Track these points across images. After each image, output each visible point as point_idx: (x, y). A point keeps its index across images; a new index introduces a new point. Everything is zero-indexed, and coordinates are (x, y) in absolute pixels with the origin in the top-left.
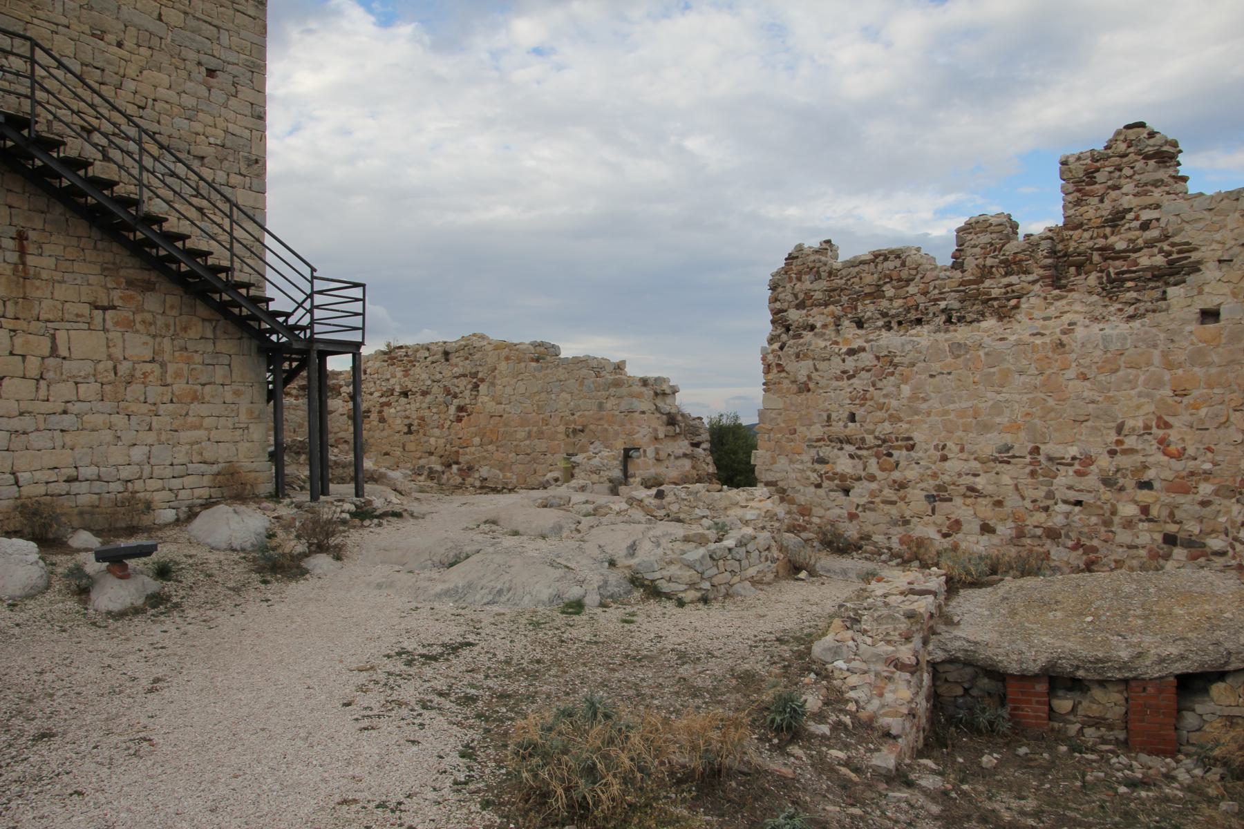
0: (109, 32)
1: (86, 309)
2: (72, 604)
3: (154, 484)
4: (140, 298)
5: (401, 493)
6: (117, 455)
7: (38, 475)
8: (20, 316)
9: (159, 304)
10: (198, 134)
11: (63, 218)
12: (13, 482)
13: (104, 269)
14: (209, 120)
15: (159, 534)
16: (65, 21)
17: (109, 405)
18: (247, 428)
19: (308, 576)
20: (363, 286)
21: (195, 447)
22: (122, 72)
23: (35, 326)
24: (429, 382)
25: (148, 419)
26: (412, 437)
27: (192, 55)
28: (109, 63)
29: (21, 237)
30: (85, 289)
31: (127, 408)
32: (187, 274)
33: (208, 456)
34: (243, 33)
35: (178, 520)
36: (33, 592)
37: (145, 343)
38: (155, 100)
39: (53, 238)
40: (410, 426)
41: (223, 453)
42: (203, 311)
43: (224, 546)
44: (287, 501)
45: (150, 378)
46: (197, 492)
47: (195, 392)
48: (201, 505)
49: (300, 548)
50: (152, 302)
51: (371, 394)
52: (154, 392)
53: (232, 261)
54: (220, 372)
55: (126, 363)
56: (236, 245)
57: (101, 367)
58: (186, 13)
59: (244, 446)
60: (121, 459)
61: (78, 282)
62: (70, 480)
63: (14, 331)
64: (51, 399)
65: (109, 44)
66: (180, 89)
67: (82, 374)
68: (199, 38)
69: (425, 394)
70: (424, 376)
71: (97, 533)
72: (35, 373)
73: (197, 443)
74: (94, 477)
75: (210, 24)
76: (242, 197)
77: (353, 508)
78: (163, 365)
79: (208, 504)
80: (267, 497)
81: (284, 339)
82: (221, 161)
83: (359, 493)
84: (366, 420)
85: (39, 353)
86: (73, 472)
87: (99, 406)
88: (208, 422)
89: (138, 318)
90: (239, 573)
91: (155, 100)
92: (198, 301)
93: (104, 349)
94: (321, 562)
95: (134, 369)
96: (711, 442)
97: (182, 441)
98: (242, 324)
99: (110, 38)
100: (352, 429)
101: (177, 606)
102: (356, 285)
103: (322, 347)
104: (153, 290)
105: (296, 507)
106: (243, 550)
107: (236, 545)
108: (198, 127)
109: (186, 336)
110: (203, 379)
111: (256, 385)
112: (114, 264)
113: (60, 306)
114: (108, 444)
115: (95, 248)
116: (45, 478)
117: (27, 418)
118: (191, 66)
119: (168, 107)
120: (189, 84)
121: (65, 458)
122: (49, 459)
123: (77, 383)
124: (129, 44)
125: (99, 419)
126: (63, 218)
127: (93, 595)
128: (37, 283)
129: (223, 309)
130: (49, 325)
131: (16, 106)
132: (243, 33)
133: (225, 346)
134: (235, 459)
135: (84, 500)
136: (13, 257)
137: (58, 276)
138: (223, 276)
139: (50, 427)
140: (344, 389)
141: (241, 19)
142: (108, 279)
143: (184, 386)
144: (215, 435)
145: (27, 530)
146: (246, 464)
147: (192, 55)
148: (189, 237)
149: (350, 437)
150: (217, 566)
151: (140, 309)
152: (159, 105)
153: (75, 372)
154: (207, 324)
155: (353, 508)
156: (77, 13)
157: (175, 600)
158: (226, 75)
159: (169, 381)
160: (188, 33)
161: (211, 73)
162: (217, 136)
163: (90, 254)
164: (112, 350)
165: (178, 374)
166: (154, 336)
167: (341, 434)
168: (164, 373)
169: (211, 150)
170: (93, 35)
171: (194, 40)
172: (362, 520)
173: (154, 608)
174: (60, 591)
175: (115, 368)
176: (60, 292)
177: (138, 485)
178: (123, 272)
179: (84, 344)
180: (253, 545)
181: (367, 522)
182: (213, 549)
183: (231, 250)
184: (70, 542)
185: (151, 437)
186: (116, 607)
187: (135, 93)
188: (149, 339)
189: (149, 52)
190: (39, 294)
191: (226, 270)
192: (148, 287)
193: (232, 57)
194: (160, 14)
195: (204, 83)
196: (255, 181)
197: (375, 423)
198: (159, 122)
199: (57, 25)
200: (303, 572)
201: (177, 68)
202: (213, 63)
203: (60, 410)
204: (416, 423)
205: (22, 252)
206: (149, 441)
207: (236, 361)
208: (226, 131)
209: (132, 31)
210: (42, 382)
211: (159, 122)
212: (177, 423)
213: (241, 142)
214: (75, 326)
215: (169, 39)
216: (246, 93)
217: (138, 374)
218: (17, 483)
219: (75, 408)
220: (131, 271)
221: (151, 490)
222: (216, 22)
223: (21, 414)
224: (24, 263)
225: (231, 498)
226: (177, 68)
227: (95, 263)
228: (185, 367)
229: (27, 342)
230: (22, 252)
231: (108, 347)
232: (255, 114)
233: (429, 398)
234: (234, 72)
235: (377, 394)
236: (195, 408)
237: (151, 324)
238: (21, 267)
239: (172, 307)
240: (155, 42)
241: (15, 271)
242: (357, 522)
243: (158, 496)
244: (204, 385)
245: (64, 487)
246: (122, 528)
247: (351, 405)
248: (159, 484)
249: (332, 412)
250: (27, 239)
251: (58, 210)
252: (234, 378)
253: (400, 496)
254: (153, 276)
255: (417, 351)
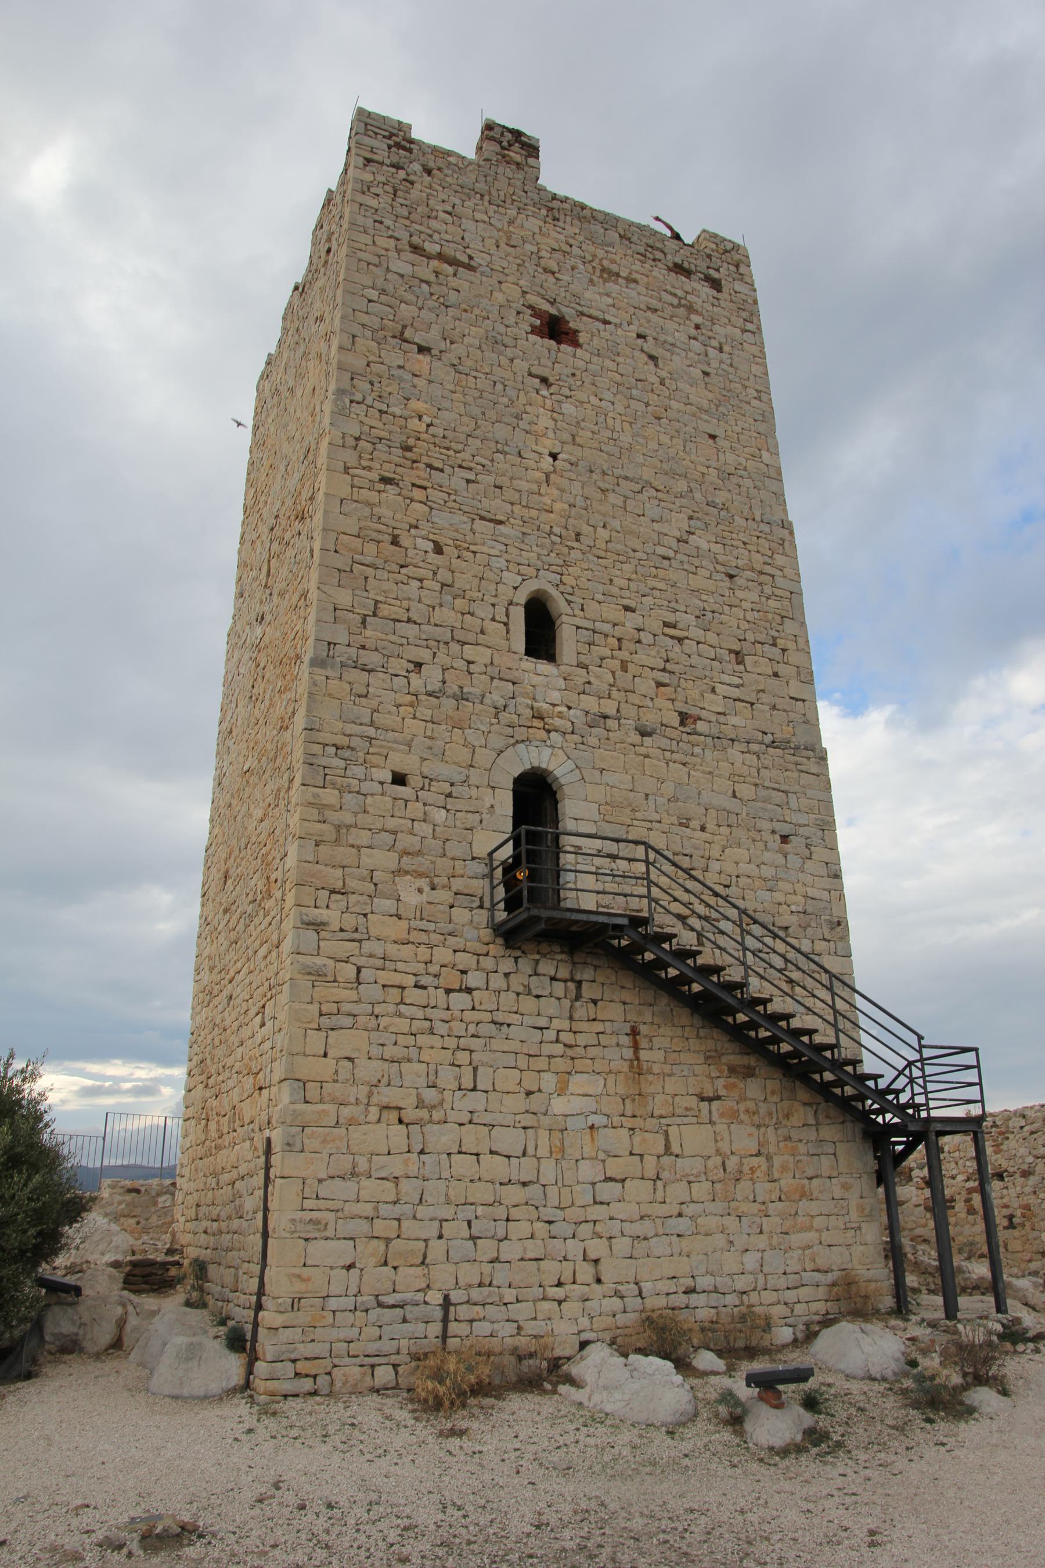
0: (695, 819)
1: (693, 1102)
2: (726, 1435)
3: (769, 1297)
4: (742, 1085)
5: (1034, 1309)
6: (731, 1262)
7: (659, 1284)
8: (637, 1113)
9: (761, 1090)
10: (780, 904)
11: (668, 1009)
12: (637, 1293)
13: (707, 1058)
14: (788, 887)
15: (780, 1356)
16: (657, 817)
17: (719, 1206)
18: (859, 1228)
19: (976, 1415)
20: (976, 1050)
21: (807, 1252)
22: (707, 855)
23: (651, 1123)
24: (1030, 1159)
25: (758, 1220)
26: (1016, 1233)
27: (766, 825)
28: (696, 849)
29: (634, 1033)
30: (692, 1080)
31: (737, 1209)
32: (789, 1055)
33: (821, 1262)
34: (810, 793)
35: (795, 1340)
36: (683, 1419)
37: (750, 1135)
38: (738, 877)
39: (661, 1030)
40: (1010, 1217)
41: (834, 1258)
42: (803, 1094)
43: (860, 1373)
44: (913, 1318)
45: (758, 1173)
46: (816, 1306)
47: (803, 1186)
48: (819, 1322)
49: (956, 1379)
50: (753, 1088)
51: (953, 1178)
52: (763, 1189)
53: (837, 1038)
54: (826, 1162)
55: (732, 1157)
56: (831, 1018)
57: (711, 1163)
58: (756, 785)
59: (858, 1250)
60: (736, 1268)
61: (685, 1073)
62: (690, 1291)
63: (633, 1129)
64: (667, 1200)
65: (694, 830)
66: (759, 861)
67: (694, 1172)
68: (770, 807)
69: (1026, 1174)
70: (1022, 1151)
71: (720, 1354)
72: (651, 1173)
73: (809, 1247)
74: (711, 1288)
75: (778, 790)
76: (832, 964)
77: (999, 1327)
78: (769, 1158)
79: (827, 1322)
80: (889, 1314)
81: (896, 1120)
82: (805, 928)
83: (1001, 1307)
84: (950, 1212)
85: (655, 1152)
86: (689, 1282)
87: (711, 1207)
88: (818, 1222)
89: (742, 1107)
90: (891, 1408)
91: (738, 877)
92: (798, 1083)
93: (713, 1144)
94: (983, 1397)
95: (741, 1164)
96: (948, 1224)
97: (793, 1246)
98: (845, 1104)
99: (695, 824)
100: (932, 1224)
101: (839, 1445)
102: (965, 1050)
103: (939, 1127)
104: (753, 1075)
105: (929, 1325)
106: (884, 1379)
107: (875, 1372)
108: (779, 897)
109: (789, 1124)
110: (810, 1173)
111: (865, 1176)
112: (716, 1051)
113: (670, 1100)
114: (722, 1249)
115: (698, 1037)
116: (665, 1290)
117: (647, 1222)
118: (766, 836)
119: (750, 881)
120: (767, 854)
121: (682, 1266)
122: (668, 1268)
123: (689, 1182)
124: (711, 826)
125: (712, 1222)
126: (668, 1009)
127: (748, 1426)
128: (650, 1077)
129: (824, 1090)
130: (663, 1121)
131: (624, 905)
132: (810, 793)
133: (829, 1132)
134: (849, 1266)
135: (704, 1314)
136: (629, 1053)
137: (667, 1069)
138: (828, 1054)
139: (667, 1231)
140: (915, 1173)
141: (805, 779)
142: (712, 1067)
143: (792, 1181)
144: (826, 1237)
145: (655, 1348)
146: (862, 1272)
147: (766, 825)
148: (794, 1016)
149: (932, 1235)
150: (862, 1397)
151: (743, 1098)
152: (743, 881)
153: (687, 1171)
154: (808, 1108)
155: (999, 1327)
156: (666, 807)
157: (836, 1437)
158: (798, 839)
159: (776, 1176)
160: (760, 804)
161: (785, 839)
162: (798, 902)
163: (694, 1044)
164: (720, 1144)
165: (784, 1168)
166: (758, 1126)
167: (919, 1231)
168: (770, 1167)
169: (794, 919)
170: (681, 824)
171: (765, 810)
172: (1014, 1344)
173: (815, 1446)
174: (709, 1420)
175: (723, 1163)
176: (672, 1085)
177: (754, 1297)
178: (724, 1059)
179: (693, 1138)
180: (895, 1374)
181: (1020, 1347)
182: (848, 1377)
183: (835, 1025)
184: (695, 1363)
185: (762, 1242)
186: (778, 1442)
187: (720, 873)
188: (753, 1130)
189: (728, 830)
190: (652, 1089)
191: (831, 1047)
192: (749, 1073)
193: (802, 819)
194: (734, 791)
195: (779, 851)
196: (840, 945)
197: (963, 1215)
198: (743, 898)
199: (651, 822)
200: (969, 1412)
201: (754, 841)
202: (785, 829)
203: (676, 1213)
204: (1018, 1213)
205: (636, 1047)
206: (761, 1246)
207: (842, 1149)
208: (806, 897)
209: (712, 812)
210: (659, 1182)
211: (743, 898)
212: (788, 1223)
213: (822, 905)
214: (686, 1120)
215: (744, 814)
216: (819, 853)
217: (746, 1169)
218: (640, 1294)
219: (689, 1210)
220: (732, 1057)
221: (764, 1302)
222: (783, 788)
223: (642, 1218)
224: (638, 1059)
225: (849, 1313)
226: (754, 841)
227: (699, 1052)
228: (791, 1159)
229: (644, 1141)
230: (636, 1047)
231: (716, 1141)
232: (832, 873)
233: (1033, 1180)
234: (806, 834)
235: (960, 1178)
236: (804, 1205)
237: (754, 1113)
238: (636, 1063)
239: (773, 1093)
240: (733, 819)
241: (631, 1067)
242: (1008, 1346)
243: (778, 1311)
244: (810, 1179)
245: (680, 1300)
246: (740, 1349)
247: (927, 1192)
248: (773, 1297)
249: (903, 1203)
250: (639, 1034)
251: (664, 1000)
252: (842, 1169)
253: (1033, 1314)
254: (752, 1060)
255: (1009, 1119)
